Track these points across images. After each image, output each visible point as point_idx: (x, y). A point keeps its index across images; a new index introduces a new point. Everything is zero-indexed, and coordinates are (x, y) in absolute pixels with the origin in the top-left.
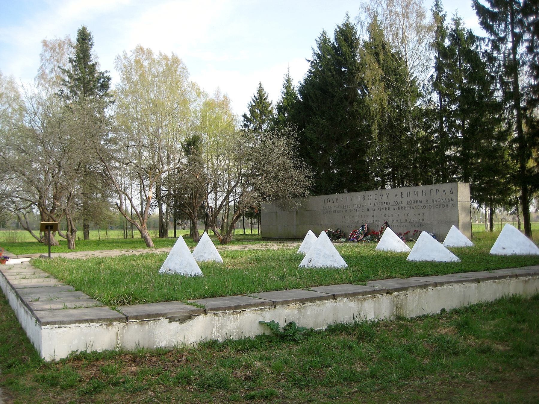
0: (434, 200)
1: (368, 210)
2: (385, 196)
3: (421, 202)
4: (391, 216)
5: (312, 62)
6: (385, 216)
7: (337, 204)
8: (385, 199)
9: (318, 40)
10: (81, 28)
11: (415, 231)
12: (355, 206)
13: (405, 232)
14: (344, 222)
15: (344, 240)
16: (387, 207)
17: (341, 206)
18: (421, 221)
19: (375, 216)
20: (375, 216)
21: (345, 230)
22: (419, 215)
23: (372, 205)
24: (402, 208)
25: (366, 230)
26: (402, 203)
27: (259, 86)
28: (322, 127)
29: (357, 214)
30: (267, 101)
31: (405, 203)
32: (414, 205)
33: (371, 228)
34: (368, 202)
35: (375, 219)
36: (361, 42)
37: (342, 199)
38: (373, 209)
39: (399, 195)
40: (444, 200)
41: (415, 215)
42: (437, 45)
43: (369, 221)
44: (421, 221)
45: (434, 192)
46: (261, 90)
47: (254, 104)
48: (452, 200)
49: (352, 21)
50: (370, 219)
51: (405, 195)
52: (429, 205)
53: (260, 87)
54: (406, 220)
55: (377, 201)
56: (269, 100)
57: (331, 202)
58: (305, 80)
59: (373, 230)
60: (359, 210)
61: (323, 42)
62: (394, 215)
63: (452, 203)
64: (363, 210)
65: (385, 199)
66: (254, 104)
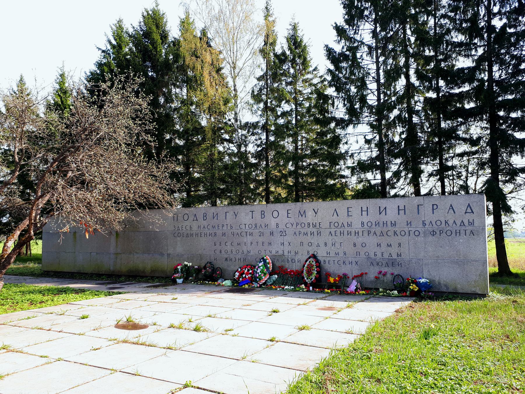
0: (427, 223)
1: (272, 234)
2: (310, 214)
3: (394, 224)
4: (322, 245)
5: (103, 51)
6: (310, 244)
7: (205, 223)
11: (380, 272)
13: (356, 273)
14: (218, 252)
16: (315, 230)
18: (395, 256)
19: (286, 243)
20: (286, 243)
25: (270, 266)
26: (349, 225)
27: (19, 79)
29: (249, 239)
31: (357, 226)
32: (378, 230)
33: (278, 264)
34: (273, 223)
35: (287, 248)
39: (342, 212)
40: (451, 222)
48: (471, 223)
49: (162, 9)
50: (276, 248)
52: (414, 230)
53: (21, 80)
55: (292, 220)
57: (191, 218)
59: (281, 268)
60: (251, 234)
61: (119, 33)
63: (469, 228)
64: (261, 234)
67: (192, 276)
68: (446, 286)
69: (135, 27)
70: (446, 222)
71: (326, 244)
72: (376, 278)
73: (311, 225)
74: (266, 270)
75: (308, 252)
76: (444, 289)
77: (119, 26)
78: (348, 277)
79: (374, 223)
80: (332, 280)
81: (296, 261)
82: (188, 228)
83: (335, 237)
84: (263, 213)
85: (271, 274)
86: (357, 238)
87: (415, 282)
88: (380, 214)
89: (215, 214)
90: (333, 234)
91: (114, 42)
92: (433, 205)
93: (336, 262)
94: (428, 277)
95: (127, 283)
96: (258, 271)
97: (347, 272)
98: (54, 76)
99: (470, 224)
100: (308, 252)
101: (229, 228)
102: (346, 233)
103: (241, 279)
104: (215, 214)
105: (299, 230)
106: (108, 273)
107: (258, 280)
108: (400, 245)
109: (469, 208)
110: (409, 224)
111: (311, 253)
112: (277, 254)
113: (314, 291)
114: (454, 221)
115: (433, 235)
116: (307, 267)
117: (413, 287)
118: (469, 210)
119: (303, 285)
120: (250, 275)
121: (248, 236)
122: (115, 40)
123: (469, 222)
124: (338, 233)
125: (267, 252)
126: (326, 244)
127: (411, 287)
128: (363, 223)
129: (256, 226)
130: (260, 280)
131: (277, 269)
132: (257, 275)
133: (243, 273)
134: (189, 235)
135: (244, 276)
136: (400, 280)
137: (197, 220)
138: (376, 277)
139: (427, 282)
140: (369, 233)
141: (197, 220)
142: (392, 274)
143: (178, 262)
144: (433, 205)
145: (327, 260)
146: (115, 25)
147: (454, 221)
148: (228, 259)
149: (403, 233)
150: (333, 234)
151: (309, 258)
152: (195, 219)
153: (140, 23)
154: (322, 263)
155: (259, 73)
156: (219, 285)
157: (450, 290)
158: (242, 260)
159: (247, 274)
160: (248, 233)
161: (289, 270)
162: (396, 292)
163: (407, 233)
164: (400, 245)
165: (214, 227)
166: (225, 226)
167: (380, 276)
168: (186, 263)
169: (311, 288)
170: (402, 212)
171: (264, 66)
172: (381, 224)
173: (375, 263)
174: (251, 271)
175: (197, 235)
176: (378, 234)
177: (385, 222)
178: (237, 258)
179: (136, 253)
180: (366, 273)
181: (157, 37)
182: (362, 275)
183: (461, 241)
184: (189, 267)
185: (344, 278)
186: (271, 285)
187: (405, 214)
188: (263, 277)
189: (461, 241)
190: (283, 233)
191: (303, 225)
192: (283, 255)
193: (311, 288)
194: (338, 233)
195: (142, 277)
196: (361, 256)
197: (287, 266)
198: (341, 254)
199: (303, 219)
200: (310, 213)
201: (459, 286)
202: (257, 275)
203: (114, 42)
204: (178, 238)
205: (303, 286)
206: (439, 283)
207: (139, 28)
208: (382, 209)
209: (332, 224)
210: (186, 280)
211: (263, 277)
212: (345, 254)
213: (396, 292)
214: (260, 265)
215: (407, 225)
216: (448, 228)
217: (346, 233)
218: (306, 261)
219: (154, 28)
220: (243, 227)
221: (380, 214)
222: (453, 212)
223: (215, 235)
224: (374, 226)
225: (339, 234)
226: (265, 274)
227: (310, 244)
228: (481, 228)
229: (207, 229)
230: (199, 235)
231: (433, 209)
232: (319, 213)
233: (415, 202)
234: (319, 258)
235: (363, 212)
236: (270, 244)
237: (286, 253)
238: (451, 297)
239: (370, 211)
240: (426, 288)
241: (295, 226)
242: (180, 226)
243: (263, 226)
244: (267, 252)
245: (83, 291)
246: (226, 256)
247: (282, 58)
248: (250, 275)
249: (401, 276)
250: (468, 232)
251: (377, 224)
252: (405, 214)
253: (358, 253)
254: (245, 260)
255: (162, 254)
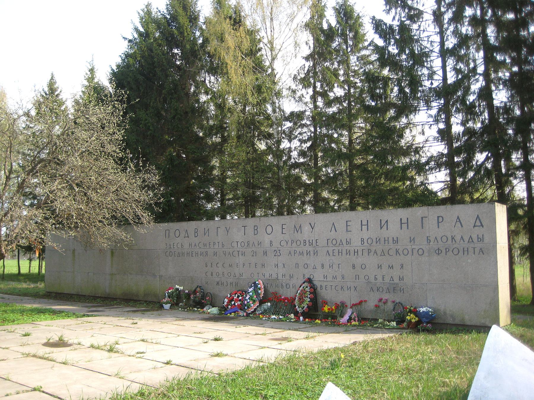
0: (432, 239)
1: (265, 253)
2: (306, 228)
3: (396, 241)
4: (319, 267)
5: (130, 41)
6: (306, 266)
8: (306, 233)
9: (142, 13)
10: (169, 360)
11: (380, 300)
12: (235, 244)
13: (356, 301)
14: (209, 274)
15: (214, 310)
16: (311, 249)
17: (205, 245)
18: (396, 280)
19: (280, 265)
20: (280, 265)
21: (211, 289)
22: (391, 267)
23: (276, 244)
24: (348, 253)
25: (262, 292)
26: (348, 243)
28: (145, 125)
29: (241, 259)
30: (60, 97)
31: (356, 243)
33: (271, 290)
34: (267, 239)
35: (281, 271)
36: (202, 20)
37: (206, 232)
38: (277, 253)
39: (341, 226)
40: (458, 238)
41: (380, 267)
42: (313, 26)
43: (267, 276)
44: (396, 280)
45: (431, 222)
46: (52, 88)
47: (42, 100)
48: (481, 239)
50: (270, 271)
51: (355, 226)
52: (417, 248)
54: (357, 277)
56: (63, 96)
57: (182, 235)
58: (118, 66)
59: (275, 294)
60: (243, 254)
61: (147, 18)
62: (327, 266)
63: (478, 246)
64: (254, 254)
65: (306, 233)
66: (42, 100)
67: (182, 302)
68: (452, 316)
69: (161, 11)
70: (453, 238)
71: (323, 266)
72: (376, 306)
73: (307, 242)
74: (255, 297)
75: (304, 276)
76: (450, 321)
77: (148, 10)
78: (346, 306)
79: (374, 240)
80: (326, 309)
81: (291, 286)
82: (179, 246)
83: (333, 258)
84: (256, 228)
85: (262, 302)
86: (357, 258)
87: (415, 312)
88: (381, 228)
89: (206, 230)
90: (331, 254)
91: (142, 30)
92: (438, 217)
93: (333, 287)
94: (432, 306)
95: (115, 306)
96: (247, 298)
97: (345, 300)
98: (84, 71)
99: (479, 240)
100: (304, 276)
101: (220, 246)
102: (344, 252)
103: (229, 307)
104: (206, 230)
105: (294, 249)
106: (104, 296)
107: (246, 308)
108: (402, 266)
109: (478, 220)
110: (412, 240)
111: (307, 276)
112: (270, 278)
113: (304, 322)
114: (462, 237)
115: (439, 254)
116: (300, 294)
117: (412, 318)
118: (478, 223)
119: (292, 315)
120: (239, 303)
121: (240, 256)
122: (143, 27)
123: (478, 238)
124: (336, 252)
125: (261, 275)
126: (323, 266)
127: (408, 318)
128: (362, 240)
129: (248, 244)
130: (248, 308)
131: (270, 296)
132: (246, 302)
133: (232, 300)
134: (181, 255)
135: (233, 303)
136: (400, 310)
137: (188, 237)
138: (376, 306)
139: (429, 311)
140: (369, 251)
141: (188, 237)
142: (393, 302)
143: (170, 286)
144: (438, 217)
145: (324, 285)
146: (143, 10)
147: (462, 237)
148: (220, 283)
149: (406, 252)
150: (331, 254)
151: (304, 283)
152: (187, 236)
153: (167, 5)
154: (319, 289)
155: (306, 51)
156: (204, 312)
157: (457, 322)
158: (234, 284)
159: (237, 300)
160: (240, 253)
161: (283, 297)
162: (394, 324)
163: (410, 252)
164: (402, 266)
165: (205, 245)
166: (217, 244)
167: (381, 304)
168: (177, 286)
169: (301, 318)
170: (405, 226)
171: (311, 43)
172: (382, 240)
173: (375, 289)
174: (240, 298)
175: (188, 254)
176: (379, 253)
177: (386, 239)
178: (229, 282)
179: (131, 274)
180: (366, 301)
181: (183, 20)
182: (361, 302)
183: (469, 261)
184: (180, 292)
185: (341, 307)
186: (259, 314)
187: (408, 228)
188: (252, 305)
189: (469, 261)
190: (277, 253)
191: (298, 243)
192: (277, 279)
193: (301, 318)
194: (336, 252)
195: (135, 301)
196: (360, 280)
197: (281, 293)
198: (339, 278)
199: (298, 236)
200: (306, 228)
201: (467, 317)
202: (246, 302)
203: (142, 30)
204: (170, 258)
205: (292, 316)
206: (445, 313)
207: (165, 11)
208: (383, 223)
209: (330, 241)
210: (175, 305)
211: (252, 305)
212: (343, 278)
213: (394, 324)
214: (250, 290)
215: (410, 242)
216: (455, 246)
217: (344, 252)
218: (300, 287)
219: (180, 11)
220: (235, 244)
221: (381, 228)
222: (460, 226)
223: (207, 254)
224: (374, 243)
225: (337, 254)
226: (254, 301)
227: (306, 266)
228: (492, 245)
229: (198, 247)
230: (191, 254)
231: (438, 222)
232: (316, 229)
233: (419, 214)
234: (315, 283)
235: (363, 227)
236: (263, 265)
237: (280, 277)
238: (454, 329)
239: (371, 225)
240: (427, 318)
241: (290, 243)
242: (172, 244)
243: (256, 244)
244: (261, 275)
245: (60, 312)
246: (217, 279)
247: (330, 34)
248: (239, 303)
249: (402, 304)
250: (477, 251)
251: (378, 241)
252: (408, 228)
253: (357, 276)
254: (237, 284)
255: (154, 276)
